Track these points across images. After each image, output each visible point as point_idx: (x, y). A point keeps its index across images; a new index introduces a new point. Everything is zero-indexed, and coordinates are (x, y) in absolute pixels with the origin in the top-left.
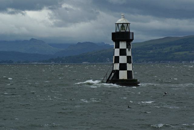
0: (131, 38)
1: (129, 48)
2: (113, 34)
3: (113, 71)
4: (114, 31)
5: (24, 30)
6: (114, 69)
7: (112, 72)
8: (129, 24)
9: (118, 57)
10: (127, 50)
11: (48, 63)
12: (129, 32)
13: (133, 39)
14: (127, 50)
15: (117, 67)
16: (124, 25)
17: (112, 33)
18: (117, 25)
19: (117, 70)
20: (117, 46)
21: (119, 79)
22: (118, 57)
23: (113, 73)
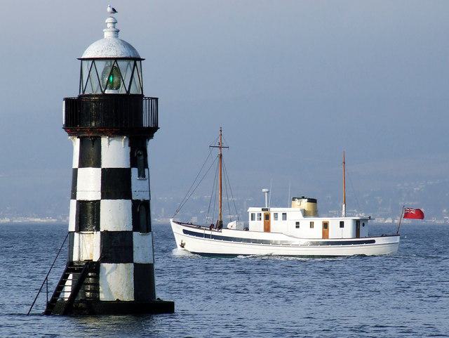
0: (146, 122)
1: (141, 163)
2: (69, 102)
3: (71, 267)
4: (74, 94)
5: (353, 229)
6: (75, 258)
7: (68, 271)
8: (138, 63)
9: (77, 169)
10: (135, 171)
11: (299, 259)
12: (142, 96)
13: (156, 128)
14: (135, 171)
15: (88, 247)
16: (121, 64)
17: (69, 102)
18: (86, 65)
19: (89, 263)
20: (90, 157)
21: (133, 300)
22: (77, 169)
23: (71, 276)
